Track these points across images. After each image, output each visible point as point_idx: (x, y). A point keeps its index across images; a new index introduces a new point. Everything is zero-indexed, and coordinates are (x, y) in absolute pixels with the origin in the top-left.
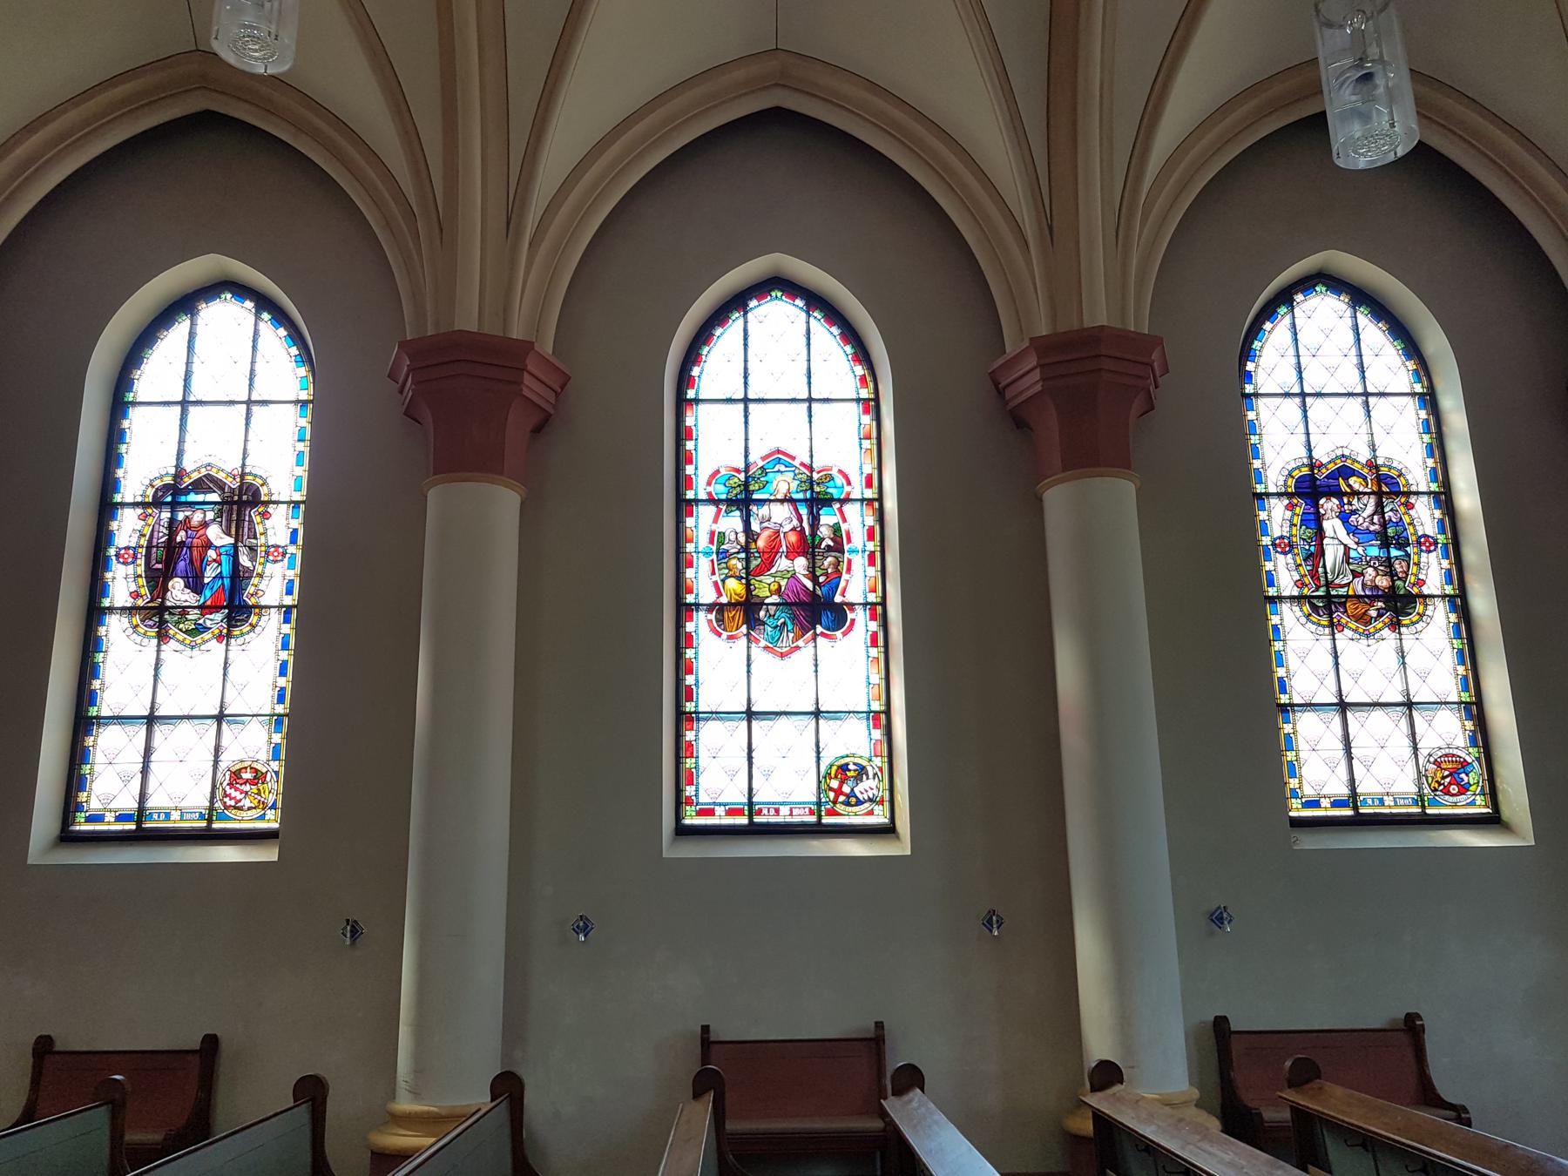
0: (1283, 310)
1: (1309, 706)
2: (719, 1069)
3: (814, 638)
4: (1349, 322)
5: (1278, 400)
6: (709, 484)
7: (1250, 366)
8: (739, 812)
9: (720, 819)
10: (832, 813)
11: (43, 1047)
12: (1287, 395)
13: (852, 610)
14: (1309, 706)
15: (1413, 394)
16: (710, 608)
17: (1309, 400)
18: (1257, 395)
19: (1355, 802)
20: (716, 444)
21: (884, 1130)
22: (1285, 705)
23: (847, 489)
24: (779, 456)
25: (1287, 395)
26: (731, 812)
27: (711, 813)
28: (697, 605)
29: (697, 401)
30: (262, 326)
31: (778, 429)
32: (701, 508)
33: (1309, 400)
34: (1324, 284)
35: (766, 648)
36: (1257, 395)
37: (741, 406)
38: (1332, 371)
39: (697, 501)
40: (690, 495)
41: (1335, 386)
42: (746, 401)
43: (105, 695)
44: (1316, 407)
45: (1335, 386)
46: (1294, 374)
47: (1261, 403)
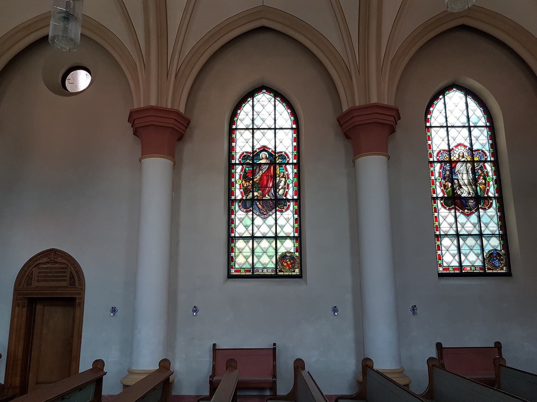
0: (441, 97)
1: (446, 235)
2: (224, 359)
3: (276, 211)
4: (273, 103)
5: (438, 129)
6: (437, 156)
7: (429, 116)
8: (249, 271)
9: (451, 271)
10: (280, 271)
11: (215, 349)
12: (442, 127)
13: (289, 202)
14: (446, 235)
15: (292, 128)
16: (442, 198)
17: (449, 129)
18: (431, 127)
19: (461, 269)
20: (438, 141)
21: (3, 385)
22: (233, 237)
23: (288, 159)
24: (264, 149)
25: (442, 127)
26: (246, 271)
27: (240, 271)
28: (235, 200)
29: (236, 129)
30: (277, 103)
31: (264, 139)
32: (237, 166)
33: (449, 129)
34: (455, 88)
35: (462, 212)
36: (431, 127)
37: (273, 131)
38: (264, 120)
39: (236, 164)
40: (233, 162)
41: (456, 123)
42: (253, 129)
43: (236, 229)
44: (452, 131)
45: (456, 123)
46: (444, 119)
47: (433, 130)
